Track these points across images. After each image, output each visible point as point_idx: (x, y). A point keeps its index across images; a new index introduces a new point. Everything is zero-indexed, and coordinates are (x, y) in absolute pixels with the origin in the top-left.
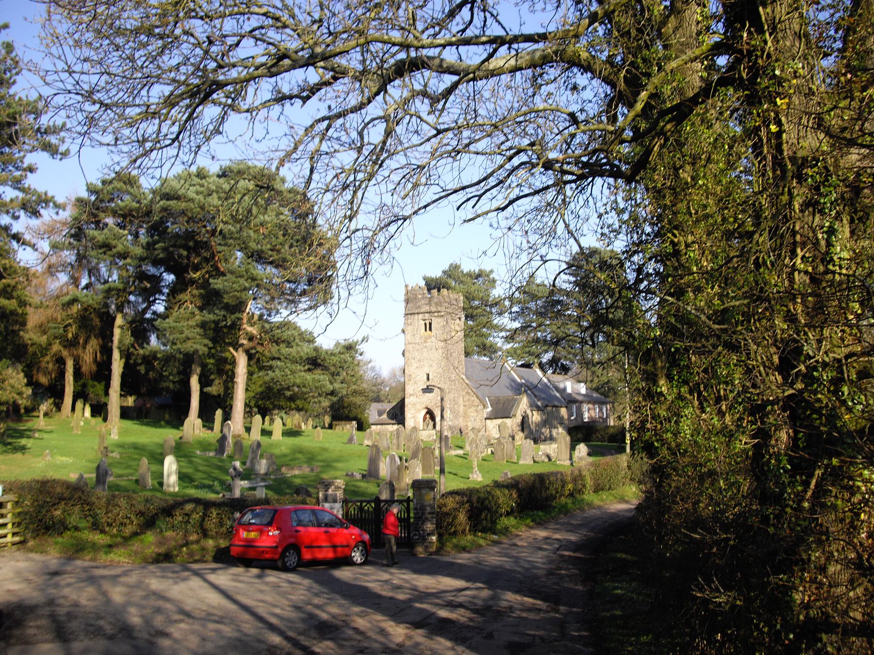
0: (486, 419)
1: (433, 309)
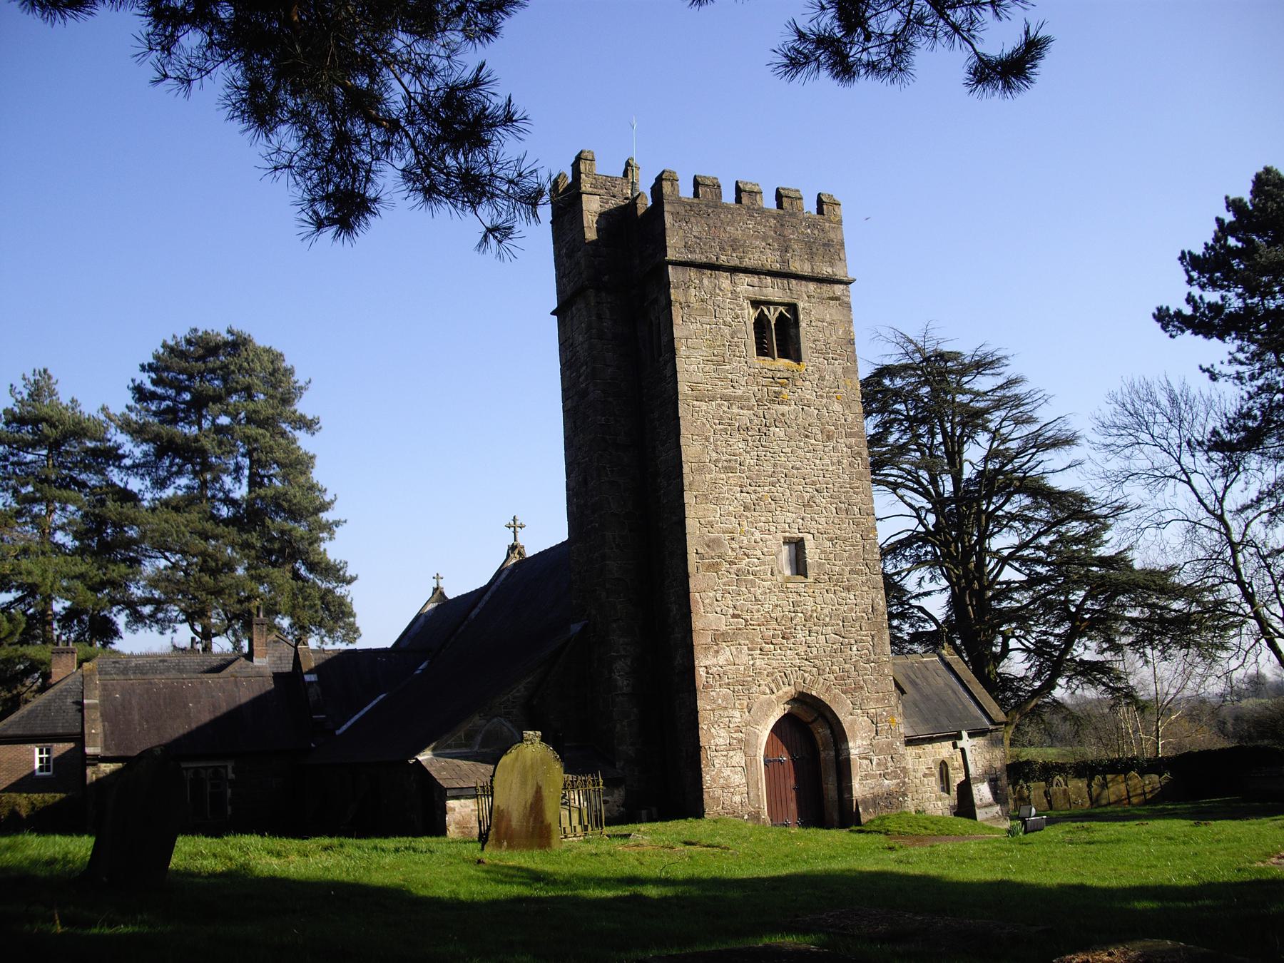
1: (796, 266)
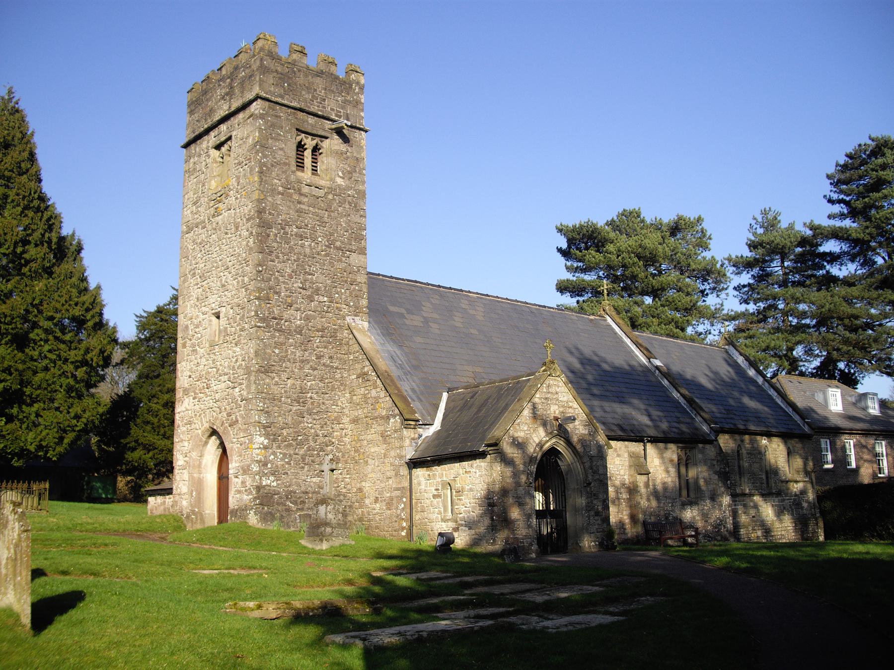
0: (414, 464)
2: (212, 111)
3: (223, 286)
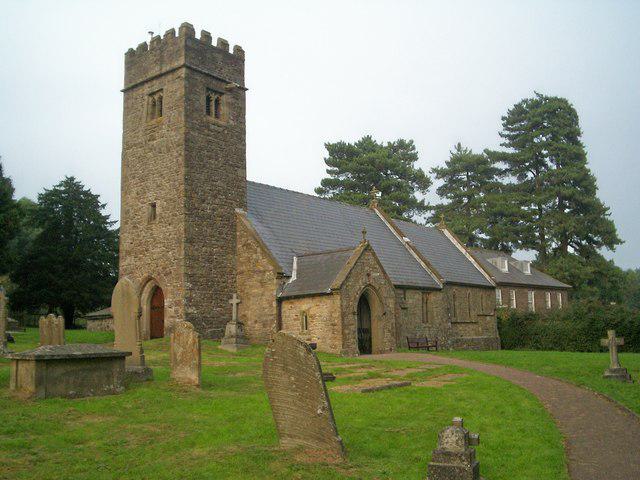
2: (146, 71)
3: (159, 186)
